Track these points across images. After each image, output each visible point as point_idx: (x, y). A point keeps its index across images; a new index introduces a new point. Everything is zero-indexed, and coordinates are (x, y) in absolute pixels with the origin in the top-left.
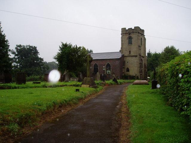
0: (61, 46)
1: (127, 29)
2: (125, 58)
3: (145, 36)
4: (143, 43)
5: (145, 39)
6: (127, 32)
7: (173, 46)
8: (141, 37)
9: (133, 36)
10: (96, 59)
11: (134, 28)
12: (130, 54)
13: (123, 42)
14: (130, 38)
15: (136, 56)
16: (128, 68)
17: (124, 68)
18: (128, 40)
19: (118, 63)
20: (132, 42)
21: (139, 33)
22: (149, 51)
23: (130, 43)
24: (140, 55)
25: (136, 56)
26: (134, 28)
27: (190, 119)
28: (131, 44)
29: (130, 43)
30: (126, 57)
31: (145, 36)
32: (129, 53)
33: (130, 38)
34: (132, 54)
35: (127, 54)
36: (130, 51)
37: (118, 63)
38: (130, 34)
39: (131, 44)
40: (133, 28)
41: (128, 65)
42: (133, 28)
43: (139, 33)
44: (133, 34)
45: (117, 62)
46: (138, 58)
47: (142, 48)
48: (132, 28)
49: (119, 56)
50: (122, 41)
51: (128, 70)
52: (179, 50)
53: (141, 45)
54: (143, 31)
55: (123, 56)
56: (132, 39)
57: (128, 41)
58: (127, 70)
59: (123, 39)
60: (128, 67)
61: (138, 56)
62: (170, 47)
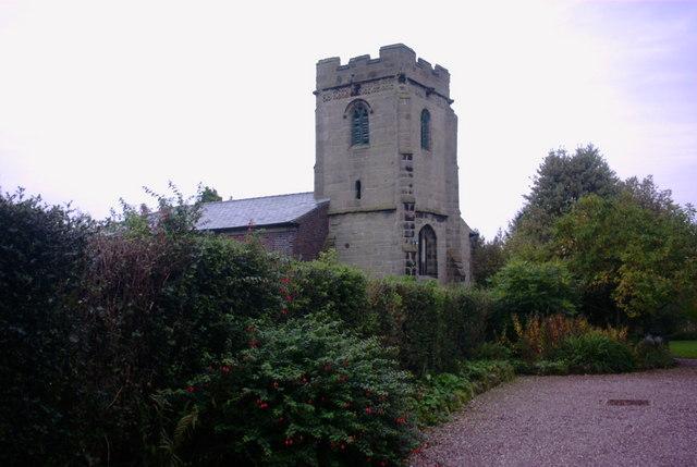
0: (528, 194)
2: (332, 221)
4: (437, 139)
5: (451, 121)
6: (345, 82)
9: (369, 96)
10: (270, 223)
11: (378, 57)
12: (359, 196)
15: (391, 211)
18: (348, 122)
21: (402, 78)
23: (360, 136)
24: (409, 205)
25: (391, 211)
26: (378, 57)
27: (696, 305)
29: (360, 136)
32: (354, 192)
34: (372, 199)
35: (342, 200)
36: (358, 185)
38: (358, 86)
39: (367, 142)
40: (375, 55)
42: (375, 55)
43: (402, 78)
44: (372, 86)
46: (397, 220)
48: (368, 56)
49: (312, 205)
52: (655, 181)
53: (425, 143)
54: (441, 74)
56: (370, 117)
59: (326, 120)
61: (401, 210)
62: (571, 153)
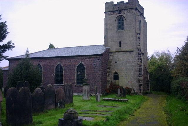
1: (115, 3)
3: (145, 18)
5: (145, 24)
6: (115, 9)
7: (13, 47)
8: (140, 18)
9: (124, 14)
12: (120, 46)
13: (108, 27)
14: (121, 19)
16: (116, 73)
17: (109, 72)
18: (117, 22)
19: (98, 62)
20: (123, 26)
22: (5, 22)
23: (121, 27)
24: (139, 50)
28: (123, 29)
29: (121, 27)
30: (112, 52)
31: (145, 18)
32: (119, 45)
33: (121, 19)
34: (124, 47)
35: (114, 47)
36: (120, 43)
37: (98, 62)
39: (123, 29)
41: (115, 68)
44: (126, 11)
45: (96, 60)
47: (142, 36)
48: (124, 2)
49: (101, 51)
50: (106, 24)
51: (116, 77)
54: (142, 9)
55: (108, 52)
56: (125, 21)
57: (116, 24)
58: (114, 76)
60: (116, 70)
